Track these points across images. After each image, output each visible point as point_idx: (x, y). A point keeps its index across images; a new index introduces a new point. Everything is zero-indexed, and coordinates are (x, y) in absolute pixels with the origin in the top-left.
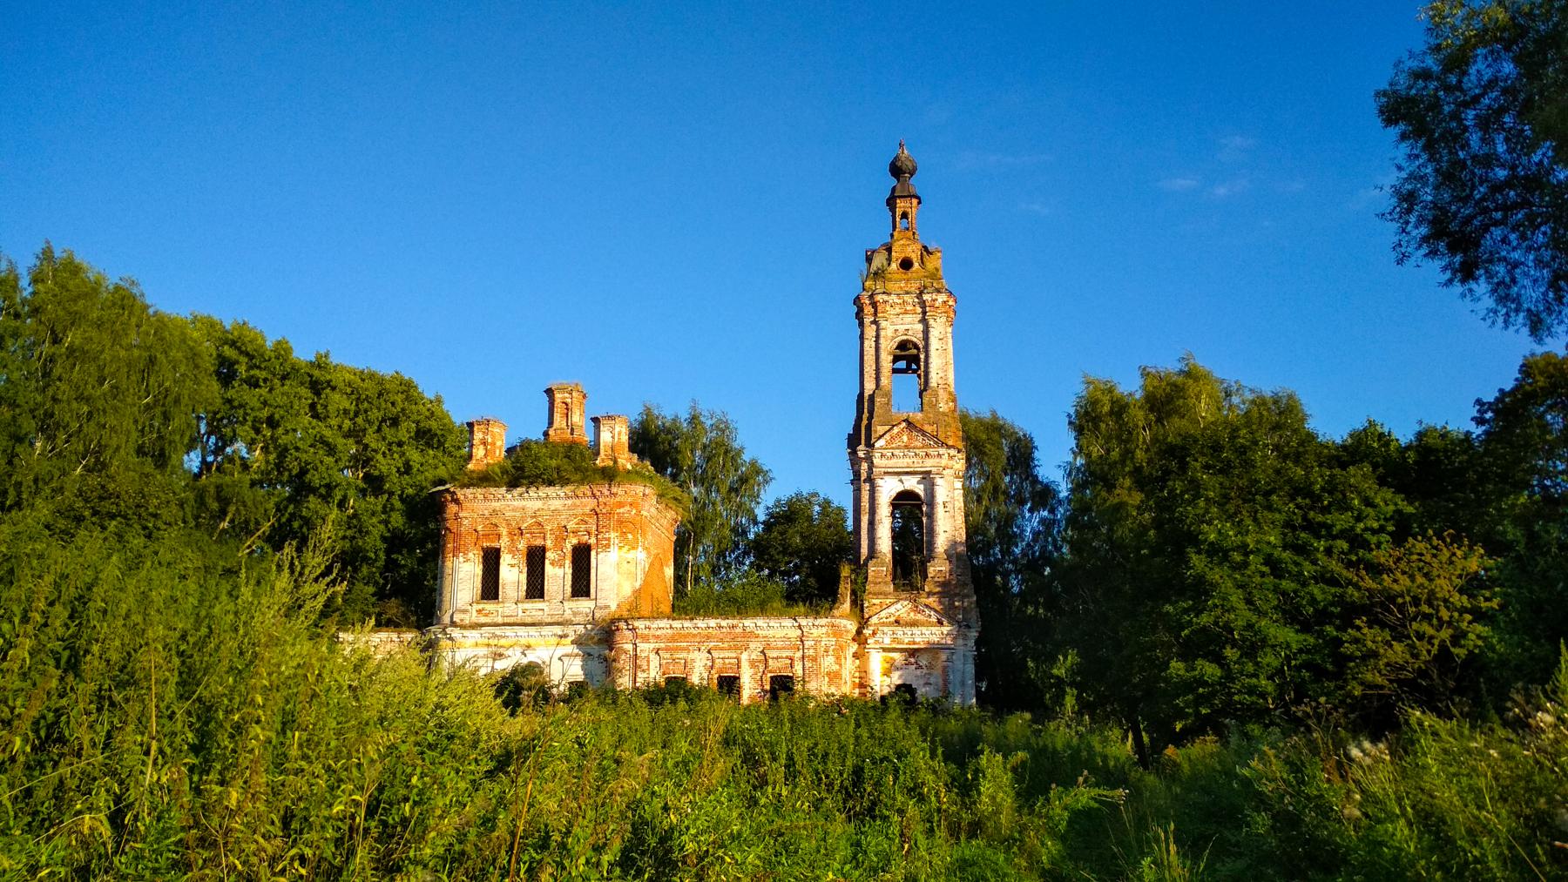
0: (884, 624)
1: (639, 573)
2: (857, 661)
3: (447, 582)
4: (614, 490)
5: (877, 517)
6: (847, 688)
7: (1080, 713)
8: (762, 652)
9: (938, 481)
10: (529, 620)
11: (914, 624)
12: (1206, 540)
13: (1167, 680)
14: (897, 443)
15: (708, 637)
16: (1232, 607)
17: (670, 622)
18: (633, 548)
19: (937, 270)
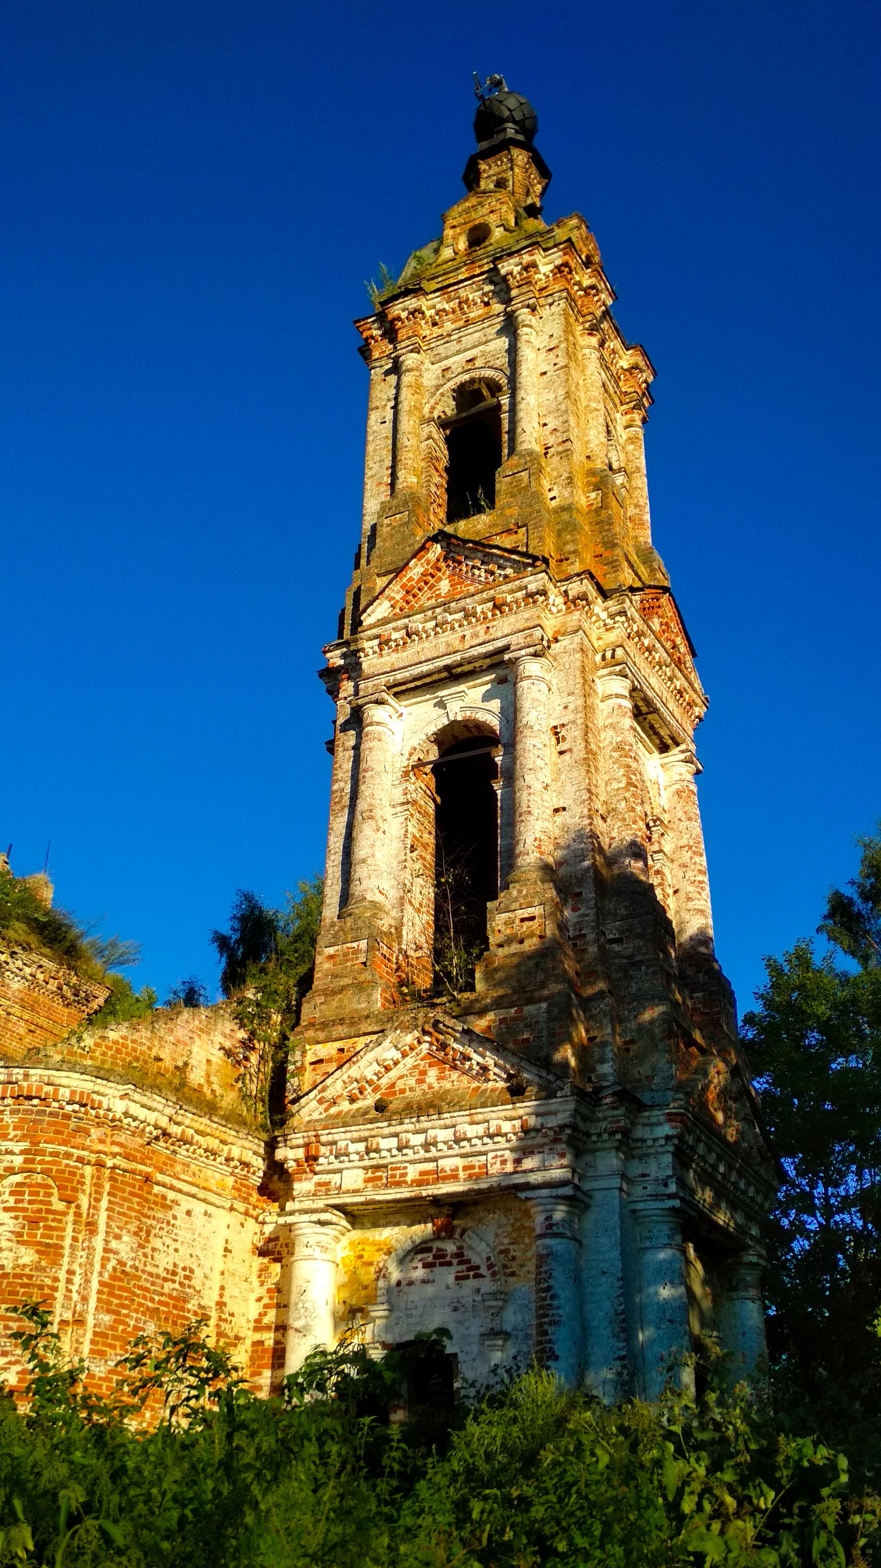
14: (425, 599)
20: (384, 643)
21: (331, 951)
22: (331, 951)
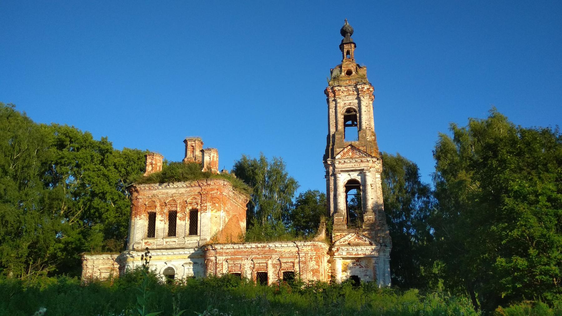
0: (342, 245)
1: (221, 222)
2: (330, 264)
3: (132, 230)
4: (209, 183)
5: (338, 193)
6: (325, 278)
7: (445, 291)
8: (279, 260)
9: (368, 174)
10: (169, 247)
11: (357, 245)
12: (512, 190)
13: (495, 269)
14: (347, 156)
15: (252, 253)
16: (531, 226)
17: (233, 245)
18: (219, 210)
19: (364, 75)
20: (339, 163)
21: (336, 218)
22: (336, 218)
